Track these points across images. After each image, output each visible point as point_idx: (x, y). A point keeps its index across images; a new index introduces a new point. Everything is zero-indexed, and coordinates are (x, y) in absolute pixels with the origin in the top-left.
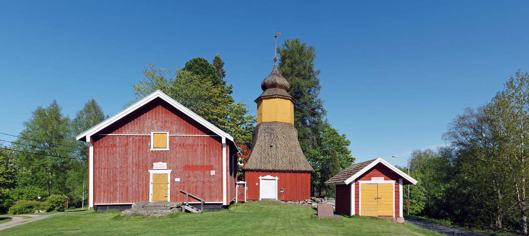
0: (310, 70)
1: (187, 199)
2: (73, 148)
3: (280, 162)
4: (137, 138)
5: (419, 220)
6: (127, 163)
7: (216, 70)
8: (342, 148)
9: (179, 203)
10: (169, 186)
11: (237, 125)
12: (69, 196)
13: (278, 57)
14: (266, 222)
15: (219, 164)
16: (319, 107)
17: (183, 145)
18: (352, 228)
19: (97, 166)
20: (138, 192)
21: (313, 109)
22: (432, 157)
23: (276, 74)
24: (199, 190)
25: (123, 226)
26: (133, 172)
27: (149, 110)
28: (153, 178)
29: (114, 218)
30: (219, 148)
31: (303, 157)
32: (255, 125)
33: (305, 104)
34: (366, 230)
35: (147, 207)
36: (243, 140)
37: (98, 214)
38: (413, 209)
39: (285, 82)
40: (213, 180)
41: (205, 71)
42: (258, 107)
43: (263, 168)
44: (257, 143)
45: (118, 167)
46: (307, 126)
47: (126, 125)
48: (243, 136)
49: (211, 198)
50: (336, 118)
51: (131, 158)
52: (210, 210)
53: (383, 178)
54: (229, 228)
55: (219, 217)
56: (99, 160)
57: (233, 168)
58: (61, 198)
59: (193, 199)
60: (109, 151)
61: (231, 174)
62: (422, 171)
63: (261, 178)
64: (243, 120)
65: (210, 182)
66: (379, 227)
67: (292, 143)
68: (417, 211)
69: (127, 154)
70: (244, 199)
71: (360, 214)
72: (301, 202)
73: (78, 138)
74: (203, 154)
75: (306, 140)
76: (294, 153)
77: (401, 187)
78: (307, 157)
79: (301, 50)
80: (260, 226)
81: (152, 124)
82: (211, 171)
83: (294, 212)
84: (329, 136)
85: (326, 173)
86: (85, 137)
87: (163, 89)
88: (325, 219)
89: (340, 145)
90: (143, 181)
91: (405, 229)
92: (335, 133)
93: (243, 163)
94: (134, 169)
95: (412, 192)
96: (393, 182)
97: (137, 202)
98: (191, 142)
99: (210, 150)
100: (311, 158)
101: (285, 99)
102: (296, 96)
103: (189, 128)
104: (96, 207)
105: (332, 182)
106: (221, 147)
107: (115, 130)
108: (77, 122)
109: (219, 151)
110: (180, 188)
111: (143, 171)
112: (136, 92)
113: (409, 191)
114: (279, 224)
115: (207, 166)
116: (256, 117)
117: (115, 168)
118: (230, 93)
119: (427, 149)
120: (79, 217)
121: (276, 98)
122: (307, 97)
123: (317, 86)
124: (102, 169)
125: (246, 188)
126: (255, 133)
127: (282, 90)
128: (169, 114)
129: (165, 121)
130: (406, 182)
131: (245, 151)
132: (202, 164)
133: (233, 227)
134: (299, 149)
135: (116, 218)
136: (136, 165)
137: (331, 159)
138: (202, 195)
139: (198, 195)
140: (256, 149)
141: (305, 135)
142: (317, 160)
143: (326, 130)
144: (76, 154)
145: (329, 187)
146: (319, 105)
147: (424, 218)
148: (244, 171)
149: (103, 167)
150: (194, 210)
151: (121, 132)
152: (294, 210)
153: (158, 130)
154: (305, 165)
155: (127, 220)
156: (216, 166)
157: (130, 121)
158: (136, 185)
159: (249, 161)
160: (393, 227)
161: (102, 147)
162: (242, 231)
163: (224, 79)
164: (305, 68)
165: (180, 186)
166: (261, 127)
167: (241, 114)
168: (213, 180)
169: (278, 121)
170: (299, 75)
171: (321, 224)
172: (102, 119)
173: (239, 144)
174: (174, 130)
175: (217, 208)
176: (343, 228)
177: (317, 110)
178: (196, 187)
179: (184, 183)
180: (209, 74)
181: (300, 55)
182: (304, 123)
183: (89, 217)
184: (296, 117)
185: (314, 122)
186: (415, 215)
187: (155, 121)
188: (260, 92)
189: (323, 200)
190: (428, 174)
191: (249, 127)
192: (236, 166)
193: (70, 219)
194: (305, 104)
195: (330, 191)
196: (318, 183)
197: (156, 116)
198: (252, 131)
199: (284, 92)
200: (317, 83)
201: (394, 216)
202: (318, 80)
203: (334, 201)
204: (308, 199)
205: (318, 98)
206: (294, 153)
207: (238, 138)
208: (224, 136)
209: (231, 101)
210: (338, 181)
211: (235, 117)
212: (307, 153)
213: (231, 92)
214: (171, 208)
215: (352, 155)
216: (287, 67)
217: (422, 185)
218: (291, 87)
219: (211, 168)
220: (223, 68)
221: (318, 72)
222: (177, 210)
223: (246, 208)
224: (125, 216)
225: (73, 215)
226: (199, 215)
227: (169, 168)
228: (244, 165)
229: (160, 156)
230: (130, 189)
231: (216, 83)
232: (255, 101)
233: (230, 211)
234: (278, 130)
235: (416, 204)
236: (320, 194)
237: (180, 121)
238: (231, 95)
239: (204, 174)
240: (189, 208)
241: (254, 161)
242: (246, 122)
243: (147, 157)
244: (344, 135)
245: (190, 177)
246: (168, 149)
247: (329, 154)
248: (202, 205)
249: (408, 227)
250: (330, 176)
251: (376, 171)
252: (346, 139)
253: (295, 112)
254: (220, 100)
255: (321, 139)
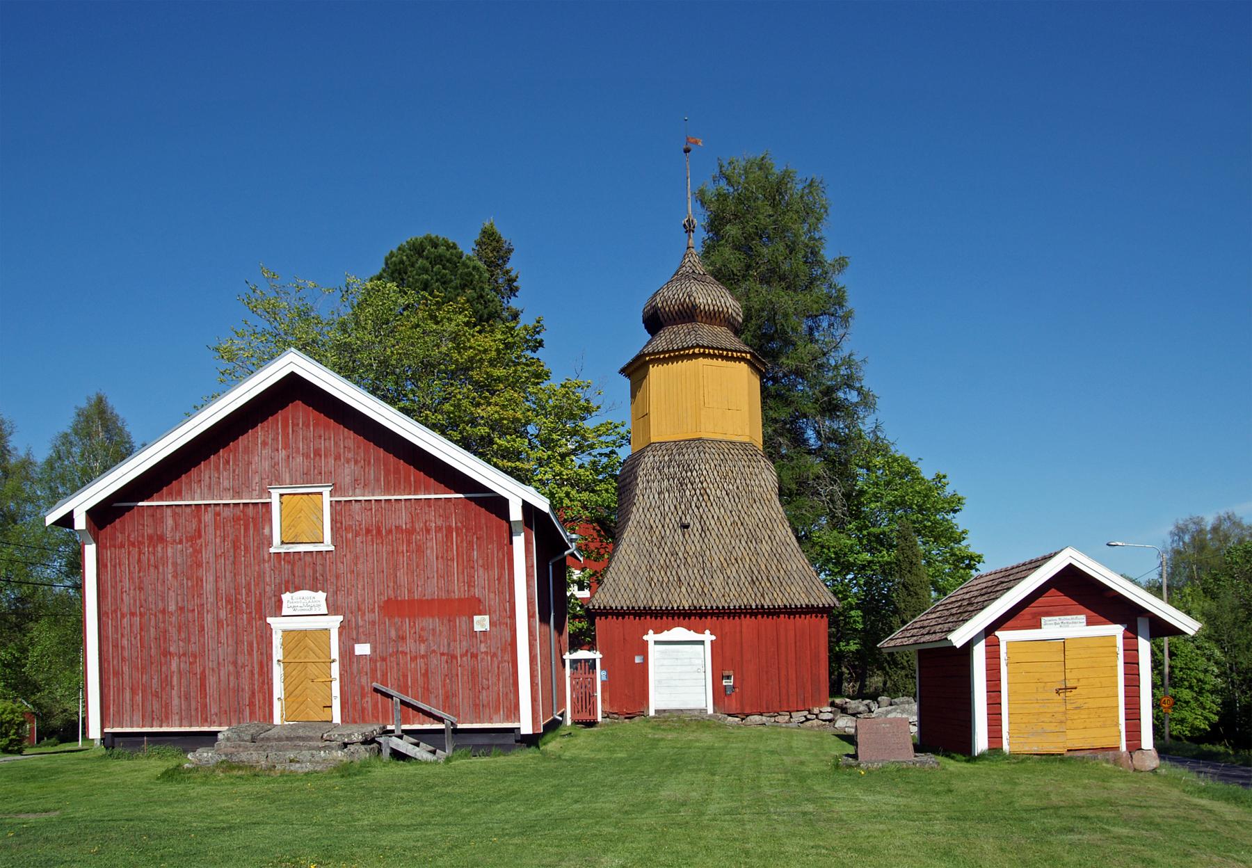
0: (813, 257)
1: (398, 715)
2: (44, 552)
3: (718, 581)
4: (226, 513)
5: (1210, 758)
6: (200, 595)
7: (487, 275)
8: (935, 523)
9: (372, 728)
10: (335, 669)
11: (563, 456)
12: (34, 704)
13: (700, 221)
14: (673, 789)
15: (501, 593)
16: (849, 382)
17: (379, 531)
18: (981, 795)
19: (109, 607)
20: (238, 690)
21: (829, 391)
22: (1240, 542)
23: (693, 276)
24: (436, 683)
25: (190, 800)
26: (220, 622)
27: (264, 419)
28: (284, 645)
29: (163, 774)
30: (500, 537)
31: (798, 561)
32: (624, 453)
33: (799, 373)
34: (1028, 801)
35: (268, 739)
36: (585, 507)
37: (117, 762)
38: (1182, 721)
39: (728, 302)
40: (483, 648)
41: (455, 282)
42: (633, 396)
43: (657, 603)
44: (636, 515)
45: (172, 608)
46: (810, 452)
47: (194, 471)
48: (585, 496)
49: (477, 710)
50: (910, 418)
51: (211, 579)
52: (476, 750)
53: (1082, 618)
54: (543, 811)
55: (507, 774)
56: (114, 587)
57: (552, 601)
58: (13, 712)
59: (420, 705)
60: (144, 558)
61: (544, 619)
62: (1205, 591)
63: (650, 637)
64: (584, 438)
65: (474, 656)
66: (1076, 789)
67: (759, 512)
68: (1194, 728)
69: (199, 565)
70: (595, 713)
71: (1006, 747)
72: (798, 716)
73: (51, 518)
74: (444, 558)
75: (806, 501)
76: (765, 547)
77: (1144, 646)
78: (812, 562)
79: (776, 192)
80: (650, 804)
81: (275, 465)
82: (476, 618)
83: (772, 752)
84: (888, 484)
85: (880, 611)
86: (72, 512)
87: (309, 348)
88: (882, 771)
89: (927, 512)
90: (250, 653)
91: (1164, 789)
92: (909, 471)
93: (589, 586)
94: (223, 614)
95: (1179, 663)
96: (1117, 630)
97: (234, 725)
98: (403, 520)
99: (470, 544)
100: (828, 560)
101: (727, 358)
102: (765, 347)
103: (397, 471)
104: (109, 740)
105: (906, 642)
106: (506, 535)
107: (159, 489)
108: (52, 468)
109: (500, 548)
110: (374, 679)
111: (250, 620)
112: (225, 365)
113: (1167, 661)
114: (717, 794)
115: (460, 600)
116: (628, 426)
117: (163, 612)
118: (534, 349)
119: (1222, 513)
120: (56, 772)
121: (695, 356)
122: (805, 350)
123: (840, 313)
124: (123, 616)
125: (600, 675)
126: (625, 483)
127: (717, 329)
128: (327, 427)
129: (317, 453)
130: (1159, 629)
131: (592, 546)
132: (444, 596)
133: (555, 807)
134: (785, 533)
135: (170, 775)
136: (229, 601)
137: (898, 563)
138: (448, 701)
139: (433, 701)
140: (630, 537)
141: (802, 483)
142: (847, 567)
143: (878, 461)
144: (51, 570)
145: (892, 659)
146: (850, 377)
147: (1221, 749)
148: (591, 614)
149: (125, 610)
150: (421, 752)
151: (179, 495)
152: (773, 745)
153: (294, 482)
154: (805, 585)
155: (204, 784)
156: (492, 600)
157: (207, 457)
158: (231, 668)
159: (608, 579)
160: (1121, 785)
161: (122, 546)
162: (583, 822)
163: (514, 303)
164: (792, 250)
165: (374, 671)
166: (648, 460)
167: (572, 416)
168: (483, 648)
169: (704, 436)
170: (772, 276)
171: (870, 790)
172: (123, 453)
173: (568, 522)
174: (348, 479)
175: (500, 746)
176: (948, 799)
177: (841, 395)
178: (426, 674)
179: (384, 659)
180: (463, 287)
181: (774, 206)
182: (798, 439)
183: (87, 772)
184: (767, 420)
185: (834, 437)
186: (1187, 738)
187: (282, 454)
188: (639, 339)
189: (874, 707)
190: (1229, 599)
191: (605, 460)
192: (563, 602)
193: (31, 775)
194: (799, 373)
195: (898, 676)
196: (853, 647)
197: (286, 435)
198: (615, 477)
199: (725, 337)
200: (840, 301)
201: (1123, 748)
202: (841, 291)
203: (915, 707)
204: (820, 705)
205: (844, 352)
206: (765, 547)
207: (566, 502)
208: (517, 495)
209: (540, 376)
210: (927, 638)
211: (554, 430)
212: (814, 544)
213: (541, 344)
214: (345, 745)
215: (972, 545)
216: (727, 251)
217: (1209, 638)
218: (748, 318)
219: (474, 606)
220: (508, 266)
221: (841, 264)
222: (363, 753)
223: (599, 744)
224: (196, 769)
225: (42, 764)
226: (437, 769)
227: (333, 609)
228: (592, 596)
229: (304, 572)
230: (212, 680)
231: (485, 318)
232: (623, 371)
233: (544, 753)
234: (707, 469)
235: (1193, 704)
236: (863, 686)
237: (367, 451)
238: (540, 353)
239: (453, 629)
240: (404, 746)
241: (625, 581)
242: (592, 447)
243: (261, 575)
244: (939, 478)
245: (403, 638)
246: (327, 546)
247: (891, 546)
248: (448, 735)
249: (1173, 782)
250: (896, 620)
251: (1054, 597)
252: (948, 491)
253: (764, 403)
254: (499, 372)
255: (862, 492)
